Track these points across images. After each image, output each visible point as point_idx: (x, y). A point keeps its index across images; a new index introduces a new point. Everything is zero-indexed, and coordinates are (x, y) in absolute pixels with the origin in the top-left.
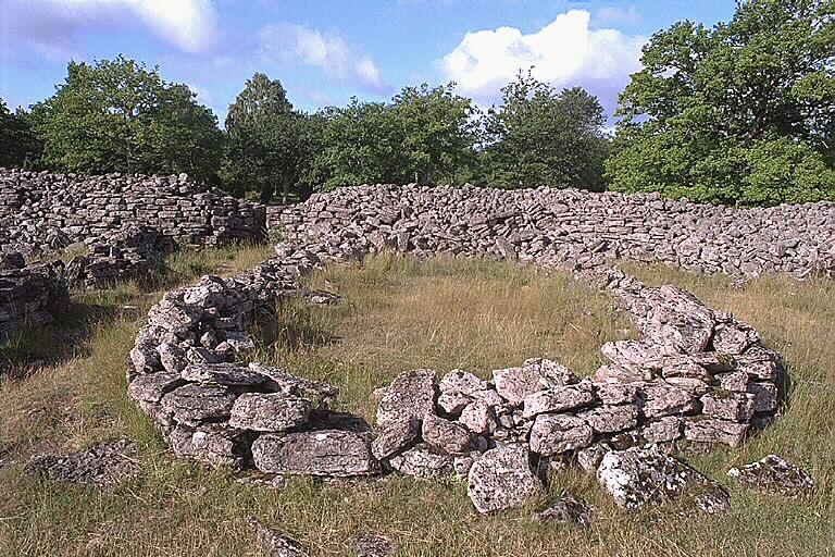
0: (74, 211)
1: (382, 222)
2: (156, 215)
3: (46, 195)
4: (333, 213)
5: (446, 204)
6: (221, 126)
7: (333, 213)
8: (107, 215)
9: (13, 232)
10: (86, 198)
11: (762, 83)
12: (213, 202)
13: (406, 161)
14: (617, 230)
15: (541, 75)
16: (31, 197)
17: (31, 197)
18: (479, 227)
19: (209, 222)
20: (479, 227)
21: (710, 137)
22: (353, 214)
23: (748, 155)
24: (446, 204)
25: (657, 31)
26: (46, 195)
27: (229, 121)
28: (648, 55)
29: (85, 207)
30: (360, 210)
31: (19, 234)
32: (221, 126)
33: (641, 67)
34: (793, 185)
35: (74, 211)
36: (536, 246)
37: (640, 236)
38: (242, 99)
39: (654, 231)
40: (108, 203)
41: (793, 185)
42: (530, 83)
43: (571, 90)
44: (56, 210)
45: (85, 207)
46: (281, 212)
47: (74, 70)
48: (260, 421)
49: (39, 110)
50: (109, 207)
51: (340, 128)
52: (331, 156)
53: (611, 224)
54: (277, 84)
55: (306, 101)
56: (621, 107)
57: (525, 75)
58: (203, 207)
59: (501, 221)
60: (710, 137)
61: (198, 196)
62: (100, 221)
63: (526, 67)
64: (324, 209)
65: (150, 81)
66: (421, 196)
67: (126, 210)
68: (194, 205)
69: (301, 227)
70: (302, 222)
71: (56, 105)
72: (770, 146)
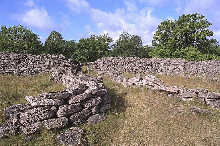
1: (120, 66)
2: (59, 65)
3: (26, 60)
5: (133, 61)
8: (46, 65)
9: (22, 70)
10: (39, 60)
13: (96, 53)
14: (175, 66)
15: (129, 32)
18: (144, 66)
19: (73, 67)
20: (144, 66)
21: (174, 47)
23: (184, 51)
26: (26, 60)
27: (46, 43)
29: (39, 63)
30: (113, 63)
33: (158, 30)
34: (197, 57)
40: (46, 62)
41: (197, 57)
42: (126, 34)
43: (135, 36)
45: (39, 63)
51: (79, 44)
53: (173, 65)
54: (58, 33)
55: (66, 38)
56: (153, 40)
57: (125, 32)
58: (71, 63)
59: (148, 65)
60: (174, 47)
62: (44, 67)
63: (125, 30)
64: (103, 63)
66: (127, 59)
67: (51, 64)
68: (68, 62)
69: (98, 68)
70: (98, 66)
72: (190, 48)
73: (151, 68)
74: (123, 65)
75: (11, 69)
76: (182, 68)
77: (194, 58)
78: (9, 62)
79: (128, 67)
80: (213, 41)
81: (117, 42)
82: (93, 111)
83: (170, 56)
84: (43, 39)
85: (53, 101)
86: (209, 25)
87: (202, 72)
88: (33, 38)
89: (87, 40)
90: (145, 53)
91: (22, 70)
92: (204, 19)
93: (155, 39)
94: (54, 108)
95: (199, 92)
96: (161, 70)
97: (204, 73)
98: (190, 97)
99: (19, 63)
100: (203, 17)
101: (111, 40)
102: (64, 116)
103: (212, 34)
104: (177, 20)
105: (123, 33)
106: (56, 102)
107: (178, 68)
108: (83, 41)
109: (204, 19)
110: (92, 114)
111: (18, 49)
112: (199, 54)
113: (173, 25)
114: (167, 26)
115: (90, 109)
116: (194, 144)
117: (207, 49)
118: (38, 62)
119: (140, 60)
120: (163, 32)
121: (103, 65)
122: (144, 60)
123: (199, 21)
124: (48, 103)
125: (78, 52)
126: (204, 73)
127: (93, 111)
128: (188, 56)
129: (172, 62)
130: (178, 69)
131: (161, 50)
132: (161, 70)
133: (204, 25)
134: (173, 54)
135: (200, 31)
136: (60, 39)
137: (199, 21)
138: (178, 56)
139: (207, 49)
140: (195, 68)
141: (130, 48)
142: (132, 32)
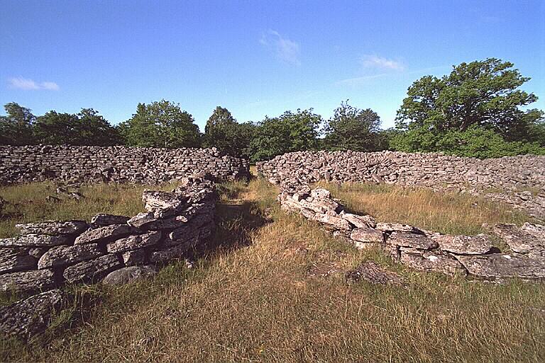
0: (169, 165)
2: (206, 167)
4: (290, 164)
5: (342, 159)
6: (202, 130)
7: (290, 164)
9: (144, 175)
11: (470, 101)
12: (231, 160)
14: (429, 169)
16: (148, 159)
17: (148, 159)
19: (230, 169)
21: (440, 128)
22: (299, 164)
24: (342, 159)
25: (415, 81)
28: (410, 91)
29: (173, 163)
31: (147, 175)
32: (202, 130)
33: (407, 96)
35: (169, 165)
36: (392, 177)
37: (440, 171)
38: (211, 118)
39: (448, 169)
40: (184, 161)
41: (490, 150)
44: (161, 165)
45: (173, 163)
46: (263, 165)
47: (141, 107)
48: (472, 248)
49: (123, 125)
50: (184, 163)
51: (260, 129)
52: (257, 142)
54: (225, 110)
55: (241, 117)
56: (398, 117)
57: (345, 103)
61: (225, 157)
63: (345, 101)
65: (177, 110)
66: (330, 156)
71: (132, 123)
73: (376, 173)
74: (322, 166)
75: (128, 173)
76: (444, 173)
77: (482, 152)
78: (128, 162)
79: (329, 171)
80: (536, 114)
81: (332, 123)
82: (126, 258)
83: (432, 148)
84: (201, 123)
85: (35, 238)
86: (523, 80)
87: (488, 180)
88: (185, 121)
89: (275, 120)
90: (379, 142)
91: (144, 175)
92: (512, 69)
93: (402, 115)
94: (35, 252)
95: (394, 231)
96: (397, 176)
97: (493, 184)
98: (368, 241)
99: (143, 163)
100: (509, 65)
101: (318, 120)
102: (46, 268)
103: (533, 98)
104: (449, 75)
105: (341, 107)
106: (42, 240)
107: (436, 172)
108: (268, 122)
109: (512, 69)
110: (122, 265)
111: (159, 141)
112: (497, 141)
113: (439, 86)
114: (426, 87)
115: (119, 255)
116: (225, 362)
117: (521, 132)
118: (172, 161)
119: (357, 156)
120: (420, 101)
121: (284, 165)
122: (364, 156)
123: (499, 74)
124: (23, 241)
125: (257, 142)
126: (493, 184)
127: (126, 258)
128: (471, 146)
129: (424, 161)
130: (435, 174)
131: (414, 135)
132: (397, 176)
133: (511, 80)
134: (437, 144)
135: (504, 94)
136: (230, 120)
137: (499, 74)
138: (447, 147)
139: (521, 132)
140: (473, 173)
141: (357, 133)
142: (359, 105)
